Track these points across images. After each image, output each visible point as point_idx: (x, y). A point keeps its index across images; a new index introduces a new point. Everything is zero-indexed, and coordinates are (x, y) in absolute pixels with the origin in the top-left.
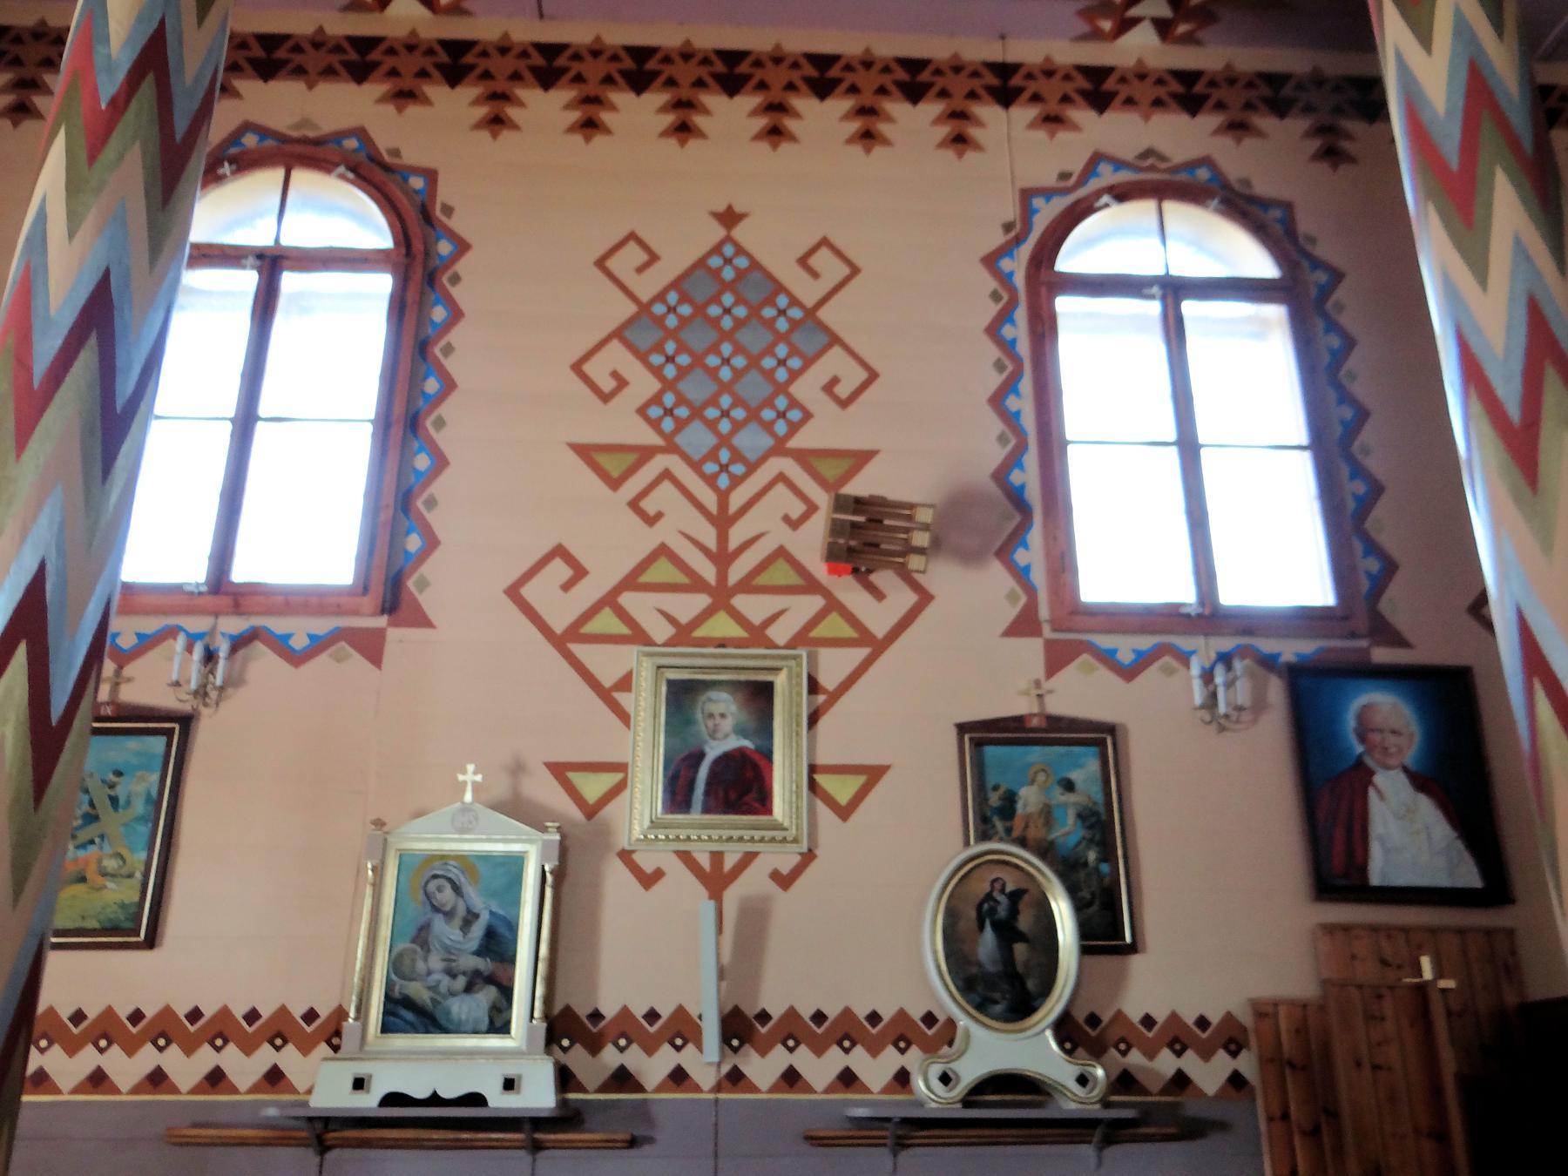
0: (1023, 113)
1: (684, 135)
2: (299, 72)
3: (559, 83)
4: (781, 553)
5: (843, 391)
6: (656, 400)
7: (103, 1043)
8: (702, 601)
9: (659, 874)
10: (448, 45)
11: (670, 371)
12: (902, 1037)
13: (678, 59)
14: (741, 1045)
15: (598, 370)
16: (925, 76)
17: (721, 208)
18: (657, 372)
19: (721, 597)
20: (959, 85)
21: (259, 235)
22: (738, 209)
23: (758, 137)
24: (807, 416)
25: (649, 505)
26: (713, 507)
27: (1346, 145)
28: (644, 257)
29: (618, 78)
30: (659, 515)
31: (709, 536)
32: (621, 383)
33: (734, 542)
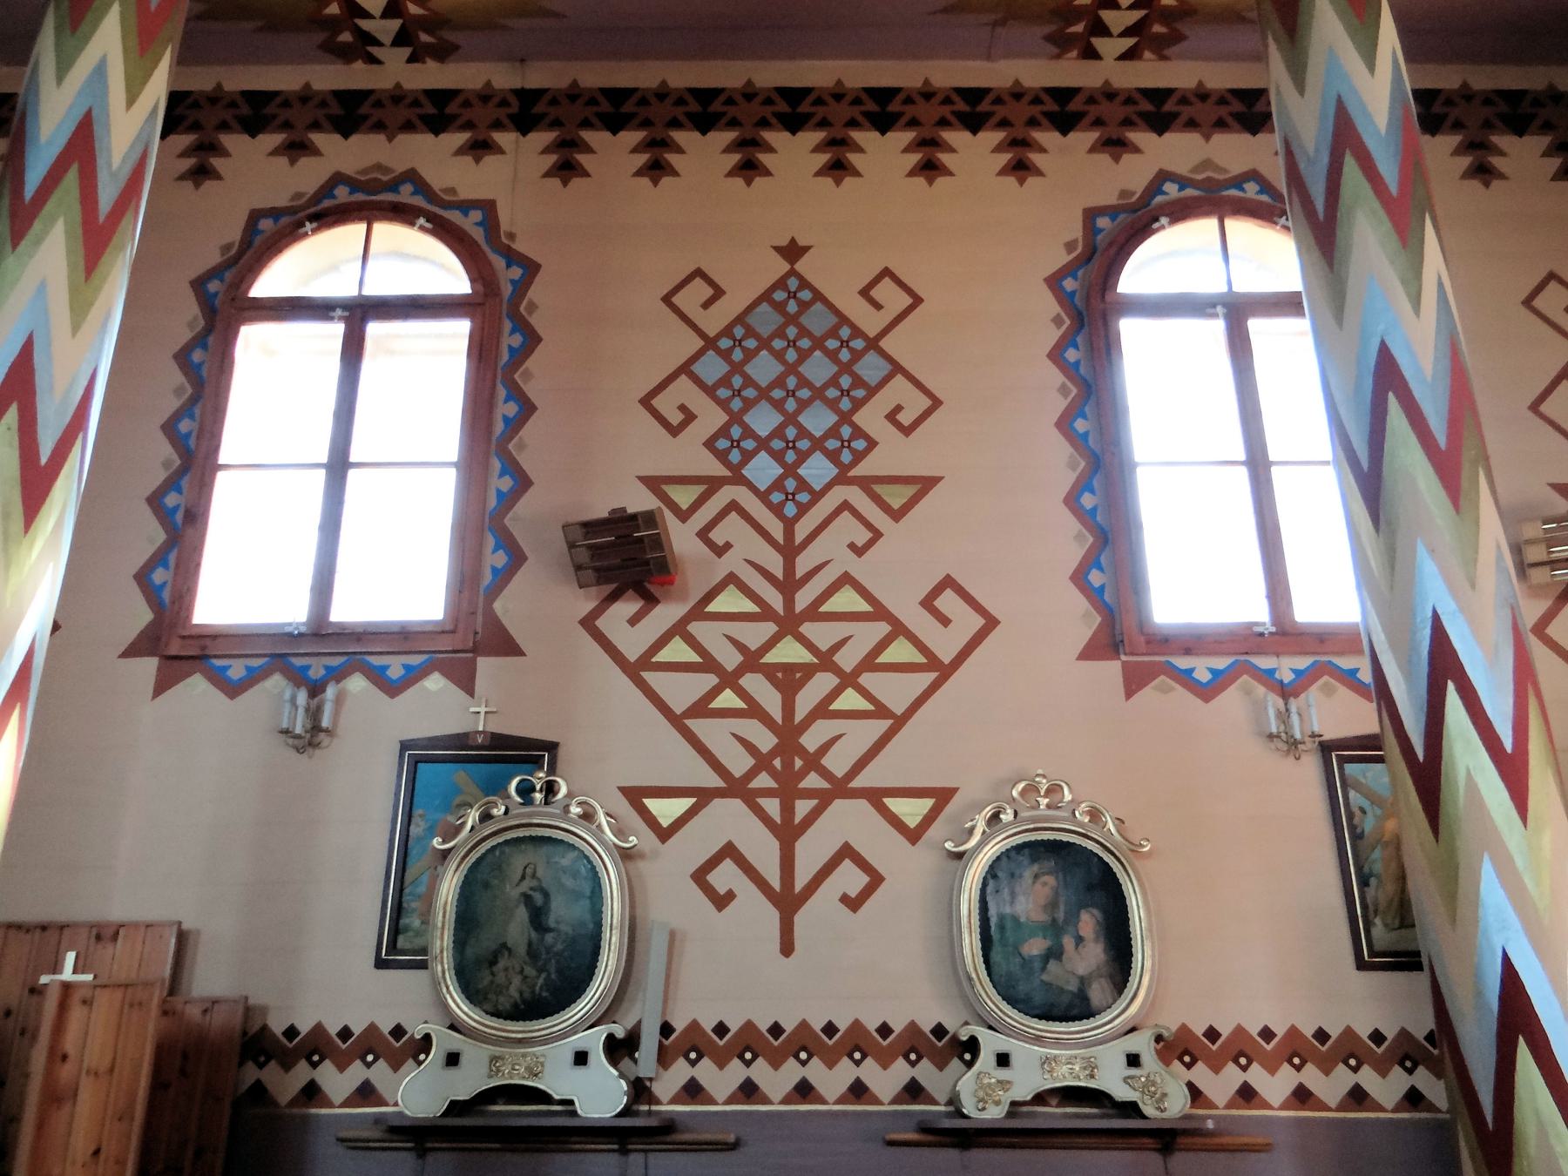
0: (1084, 138)
1: (1021, 173)
2: (379, 127)
4: (846, 580)
5: (906, 418)
6: (723, 432)
7: (803, 1055)
8: (770, 628)
9: (730, 896)
10: (339, 95)
11: (736, 404)
12: (1406, 1057)
13: (653, 100)
14: (375, 1060)
15: (666, 404)
16: (1169, 106)
17: (784, 242)
18: (724, 404)
19: (789, 625)
20: (483, 114)
21: (341, 286)
22: (802, 242)
23: (1004, 172)
24: (872, 444)
25: (718, 536)
26: (779, 536)
27: (1496, 161)
28: (709, 292)
30: (728, 546)
31: (774, 562)
32: (689, 417)
33: (800, 572)
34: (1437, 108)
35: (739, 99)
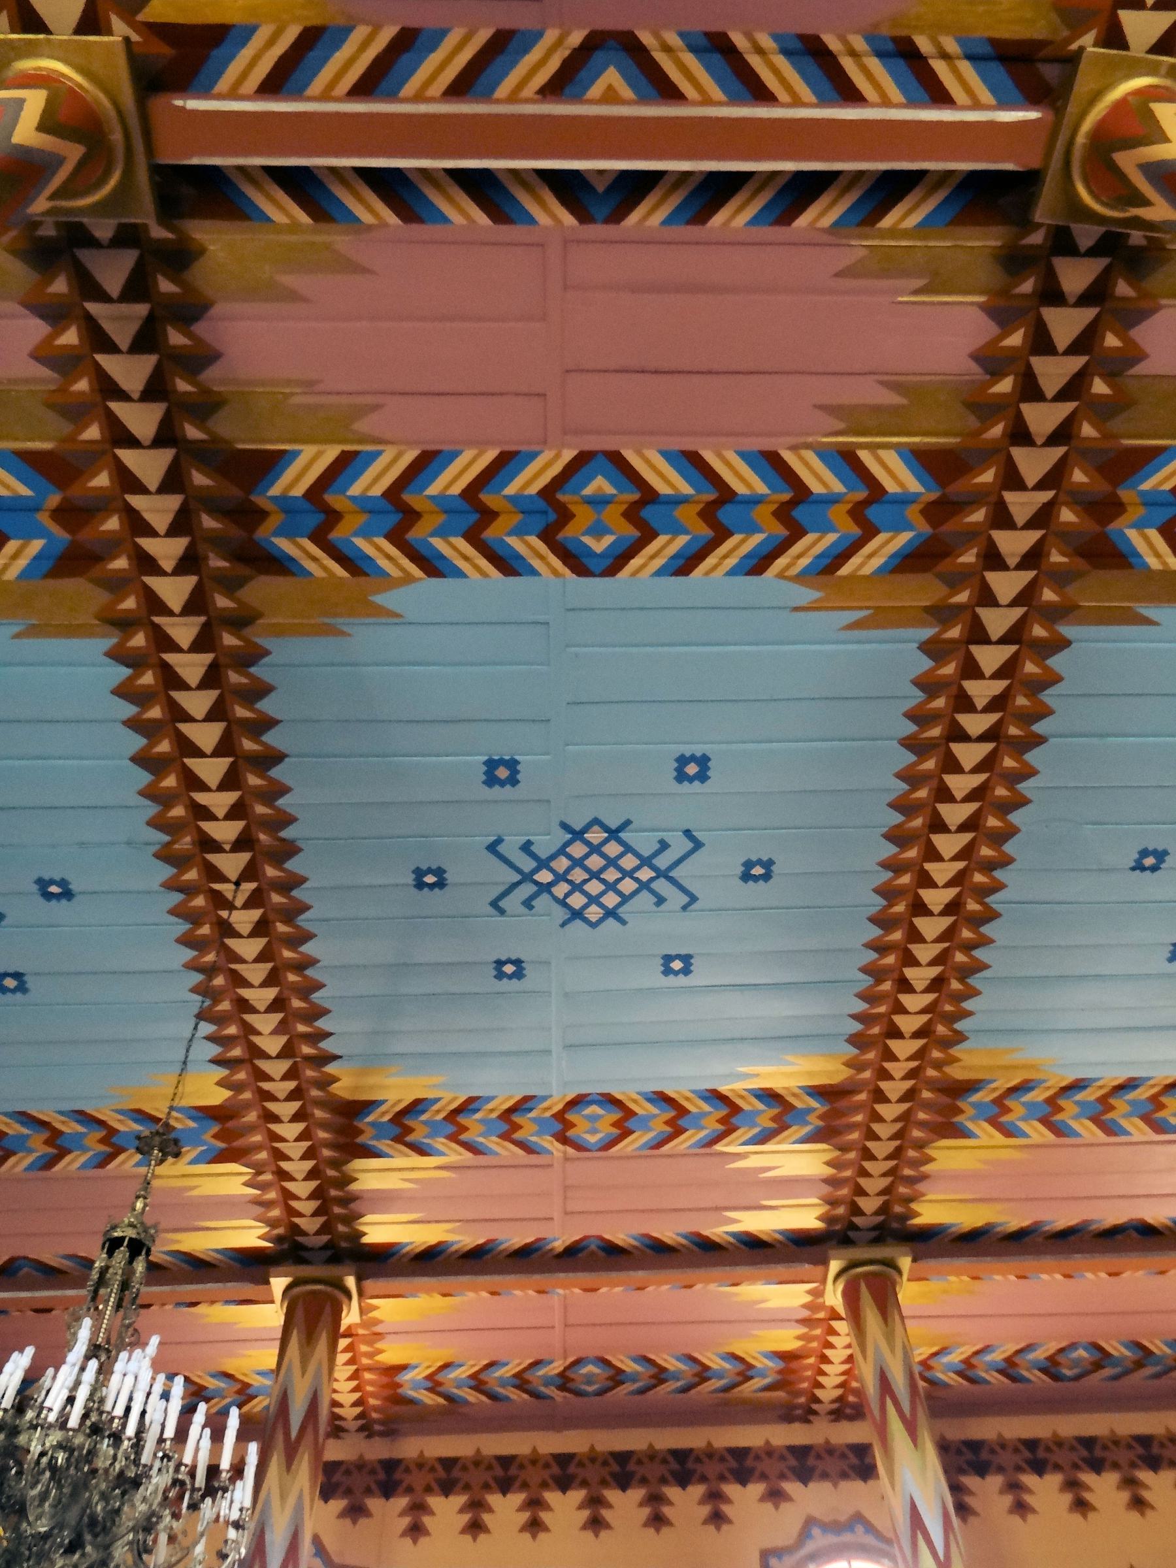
0: (756, 1489)
3: (573, 1485)
10: (792, 1449)
13: (472, 1467)
20: (534, 1475)
29: (727, 1475)
34: (337, 1477)
35: (646, 1460)
